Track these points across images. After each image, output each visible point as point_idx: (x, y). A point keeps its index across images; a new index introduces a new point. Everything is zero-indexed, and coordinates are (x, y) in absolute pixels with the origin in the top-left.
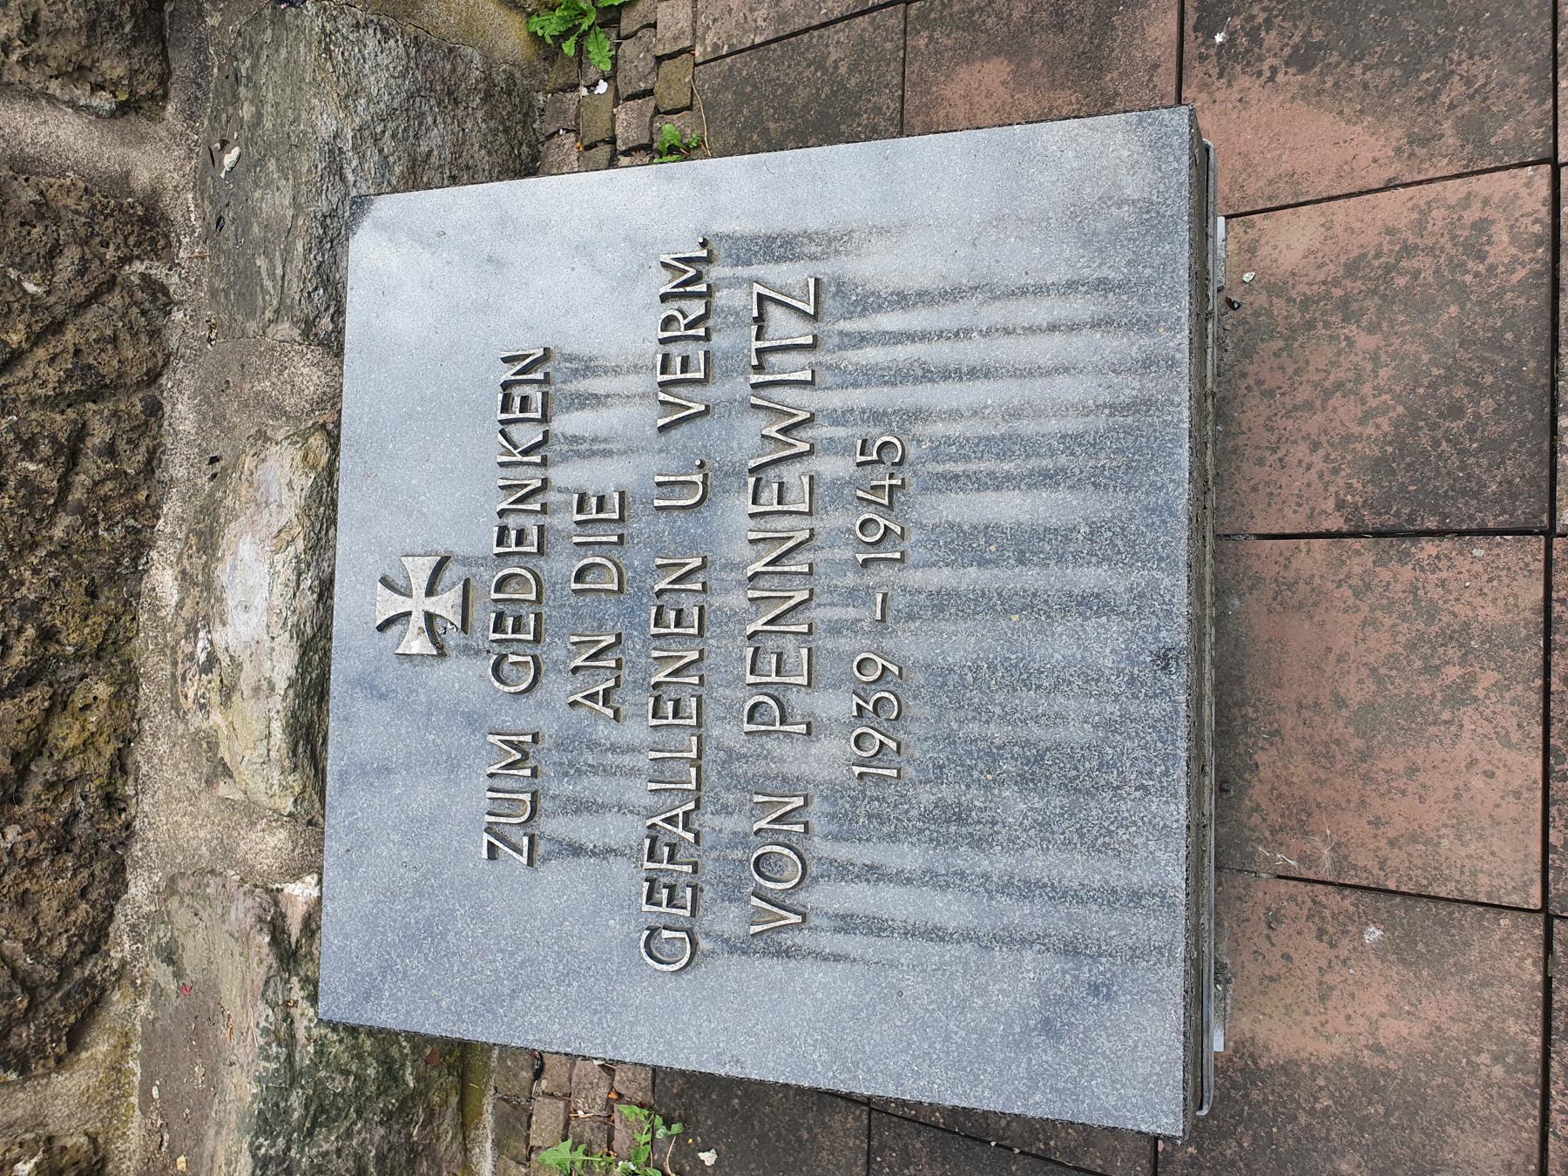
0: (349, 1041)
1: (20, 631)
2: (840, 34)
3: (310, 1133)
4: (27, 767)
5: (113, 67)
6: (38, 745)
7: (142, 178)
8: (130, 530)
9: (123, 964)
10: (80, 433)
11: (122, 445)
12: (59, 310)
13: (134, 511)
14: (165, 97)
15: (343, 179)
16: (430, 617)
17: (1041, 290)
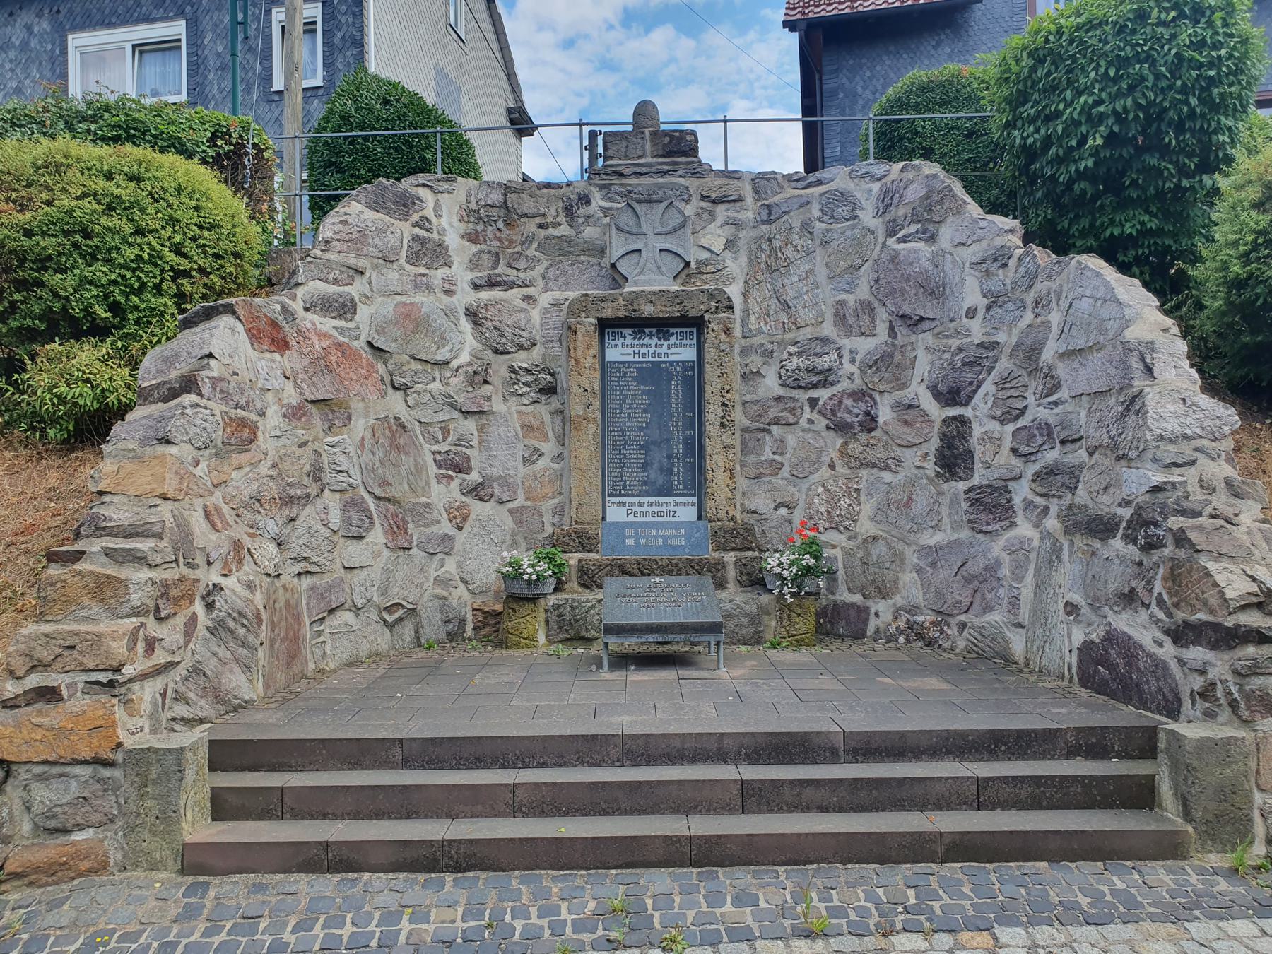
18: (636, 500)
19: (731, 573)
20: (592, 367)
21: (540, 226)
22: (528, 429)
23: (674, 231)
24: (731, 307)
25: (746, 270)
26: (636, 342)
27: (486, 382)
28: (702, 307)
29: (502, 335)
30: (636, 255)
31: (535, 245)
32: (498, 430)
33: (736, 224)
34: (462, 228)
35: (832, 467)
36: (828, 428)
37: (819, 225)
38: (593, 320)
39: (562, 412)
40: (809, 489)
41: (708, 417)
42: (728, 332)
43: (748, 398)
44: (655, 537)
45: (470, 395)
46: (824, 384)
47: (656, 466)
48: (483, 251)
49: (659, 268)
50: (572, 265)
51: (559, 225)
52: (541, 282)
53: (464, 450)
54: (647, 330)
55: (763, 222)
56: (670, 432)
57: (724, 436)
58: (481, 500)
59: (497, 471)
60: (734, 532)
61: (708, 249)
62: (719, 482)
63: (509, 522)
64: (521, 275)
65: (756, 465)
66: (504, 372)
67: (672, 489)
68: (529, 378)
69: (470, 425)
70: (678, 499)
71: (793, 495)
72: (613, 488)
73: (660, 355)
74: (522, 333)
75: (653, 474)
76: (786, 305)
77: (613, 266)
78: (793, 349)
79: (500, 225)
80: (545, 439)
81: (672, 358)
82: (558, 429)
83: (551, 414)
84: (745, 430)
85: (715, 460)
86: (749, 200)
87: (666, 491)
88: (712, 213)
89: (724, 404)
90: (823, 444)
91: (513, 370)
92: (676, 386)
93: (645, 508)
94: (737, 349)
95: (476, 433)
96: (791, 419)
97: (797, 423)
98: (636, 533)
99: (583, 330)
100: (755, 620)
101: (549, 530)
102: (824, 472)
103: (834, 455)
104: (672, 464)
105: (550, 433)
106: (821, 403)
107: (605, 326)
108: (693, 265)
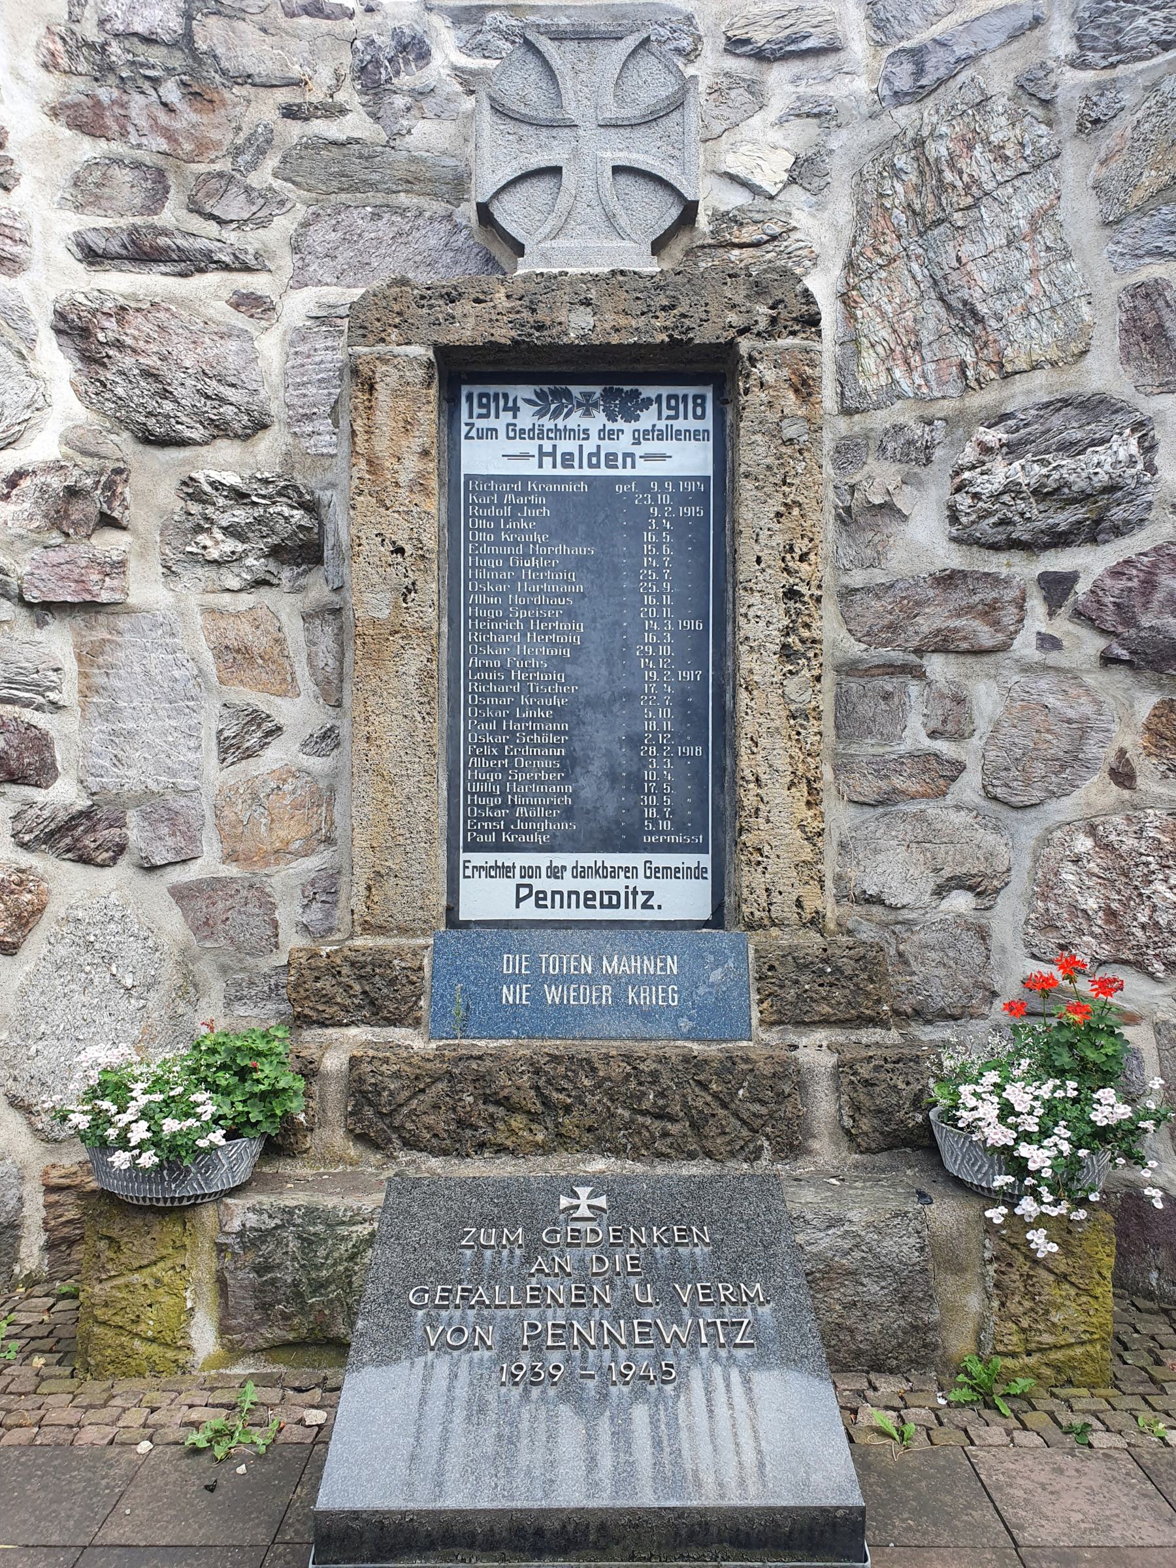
0: (346, 1255)
1: (569, 1096)
2: (990, 1515)
3: (300, 1237)
4: (501, 1105)
5: (865, 1124)
6: (512, 1108)
7: (815, 1145)
8: (625, 1146)
9: (395, 1158)
10: (673, 1119)
11: (669, 1140)
12: (733, 1106)
13: (635, 1148)
14: (861, 1152)
15: (829, 1227)
16: (577, 1207)
17: (756, 1438)
18: (541, 860)
19: (824, 1106)
20: (419, 485)
21: (290, 112)
22: (236, 657)
23: (651, 119)
24: (812, 321)
25: (848, 233)
26: (547, 423)
27: (108, 521)
28: (732, 317)
29: (165, 394)
30: (544, 185)
31: (272, 162)
32: (135, 656)
33: (821, 115)
34: (52, 86)
35: (1123, 775)
36: (1108, 660)
37: (1073, 77)
38: (421, 351)
39: (337, 612)
40: (1046, 841)
41: (747, 628)
42: (804, 388)
43: (857, 578)
44: (590, 980)
45: (54, 557)
46: (1093, 532)
48: (118, 161)
49: (610, 218)
50: (375, 216)
51: (343, 111)
52: (286, 262)
53: (28, 715)
54: (576, 390)
55: (899, 97)
57: (792, 685)
58: (85, 860)
59: (136, 775)
60: (825, 969)
61: (744, 184)
62: (776, 814)
63: (173, 924)
64: (231, 236)
65: (881, 767)
66: (168, 496)
68: (241, 515)
69: (57, 643)
70: (661, 860)
71: (990, 856)
72: (481, 825)
73: (611, 459)
74: (228, 393)
75: (589, 786)
76: (968, 317)
77: (484, 211)
78: (993, 436)
79: (171, 92)
80: (287, 688)
81: (644, 469)
82: (326, 660)
83: (306, 617)
84: (849, 668)
85: (766, 751)
86: (858, 47)
87: (625, 837)
88: (753, 88)
89: (791, 594)
90: (1088, 709)
91: (192, 491)
92: (657, 549)
93: (567, 883)
94: (828, 440)
95: (71, 666)
96: (986, 636)
97: (1004, 648)
98: (534, 964)
99: (393, 380)
100: (912, 1287)
101: (292, 941)
102: (1096, 791)
103: (1131, 740)
104: (644, 763)
105: (302, 672)
106: (1082, 587)
108: (703, 221)
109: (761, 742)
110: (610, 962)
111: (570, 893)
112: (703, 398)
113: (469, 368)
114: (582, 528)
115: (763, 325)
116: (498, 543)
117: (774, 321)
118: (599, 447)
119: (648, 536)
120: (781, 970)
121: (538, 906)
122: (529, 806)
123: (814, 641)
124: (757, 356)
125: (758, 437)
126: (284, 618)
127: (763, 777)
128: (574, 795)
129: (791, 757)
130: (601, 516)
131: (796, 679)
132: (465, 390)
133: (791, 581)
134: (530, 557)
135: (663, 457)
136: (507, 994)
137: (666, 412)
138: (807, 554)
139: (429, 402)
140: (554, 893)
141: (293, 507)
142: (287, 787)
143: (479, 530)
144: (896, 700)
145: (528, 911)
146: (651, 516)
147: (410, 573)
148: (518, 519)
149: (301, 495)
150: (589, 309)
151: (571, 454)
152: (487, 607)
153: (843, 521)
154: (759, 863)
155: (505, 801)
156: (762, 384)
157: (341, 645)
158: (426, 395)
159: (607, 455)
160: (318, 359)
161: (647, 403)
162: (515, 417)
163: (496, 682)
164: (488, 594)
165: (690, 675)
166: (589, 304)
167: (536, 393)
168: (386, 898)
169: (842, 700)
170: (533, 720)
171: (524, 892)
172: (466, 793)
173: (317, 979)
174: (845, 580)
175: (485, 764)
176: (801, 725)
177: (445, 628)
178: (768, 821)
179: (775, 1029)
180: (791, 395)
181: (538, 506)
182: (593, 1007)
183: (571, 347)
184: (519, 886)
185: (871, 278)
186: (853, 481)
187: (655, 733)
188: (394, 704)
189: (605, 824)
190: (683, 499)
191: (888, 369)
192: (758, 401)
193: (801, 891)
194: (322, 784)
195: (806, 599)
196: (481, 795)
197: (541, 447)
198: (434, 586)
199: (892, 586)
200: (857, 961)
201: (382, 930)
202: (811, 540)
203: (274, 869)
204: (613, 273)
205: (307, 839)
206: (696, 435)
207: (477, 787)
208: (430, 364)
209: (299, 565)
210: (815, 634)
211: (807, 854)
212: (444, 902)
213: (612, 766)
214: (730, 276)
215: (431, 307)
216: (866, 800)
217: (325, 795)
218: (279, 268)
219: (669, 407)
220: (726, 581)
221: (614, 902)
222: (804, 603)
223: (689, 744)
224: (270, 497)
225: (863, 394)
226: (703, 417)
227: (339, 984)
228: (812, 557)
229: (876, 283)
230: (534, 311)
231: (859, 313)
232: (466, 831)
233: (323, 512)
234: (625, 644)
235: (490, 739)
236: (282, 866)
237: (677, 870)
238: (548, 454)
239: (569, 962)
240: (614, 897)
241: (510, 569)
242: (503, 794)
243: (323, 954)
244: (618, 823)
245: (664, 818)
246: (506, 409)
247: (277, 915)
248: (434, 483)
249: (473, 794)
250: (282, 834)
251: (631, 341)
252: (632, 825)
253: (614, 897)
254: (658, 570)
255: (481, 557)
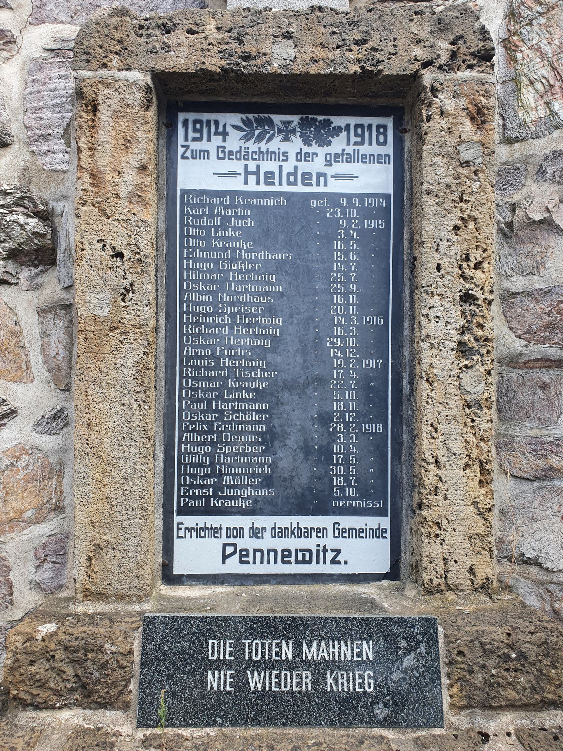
20: (136, 196)
26: (252, 146)
39: (68, 307)
41: (428, 328)
43: (518, 284)
47: (292, 441)
54: (277, 119)
56: (327, 361)
57: (467, 378)
67: (331, 497)
70: (347, 522)
72: (191, 492)
73: (307, 178)
75: (286, 459)
80: (23, 374)
81: (335, 187)
82: (57, 349)
83: (42, 312)
84: (512, 361)
92: (345, 257)
98: (239, 648)
99: (114, 102)
104: (333, 438)
105: (36, 360)
107: (181, 99)
109: (441, 428)
110: (309, 648)
111: (269, 551)
112: (385, 127)
113: (187, 98)
114: (281, 237)
115: (444, 58)
116: (208, 249)
117: (454, 55)
118: (296, 167)
119: (338, 245)
120: (469, 656)
121: (241, 562)
122: (234, 475)
123: (487, 340)
124: (439, 87)
125: (439, 159)
126: (21, 313)
127: (442, 459)
128: (273, 466)
129: (466, 442)
130: (297, 228)
131: (471, 373)
132: (182, 116)
133: (467, 286)
134: (236, 261)
135: (350, 177)
136: (213, 681)
137: (353, 139)
138: (481, 263)
139: (146, 123)
140: (255, 551)
141: (29, 216)
142: (21, 464)
143: (193, 237)
144: (553, 390)
145: (233, 566)
146: (339, 227)
147: (128, 276)
148: (226, 229)
149: (36, 205)
150: (290, 42)
151: (272, 173)
152: (199, 303)
153: (505, 235)
154: (437, 536)
155: (214, 470)
156: (442, 113)
157: (71, 336)
158: (144, 117)
159: (303, 174)
160: (52, 86)
161: (338, 130)
162: (224, 140)
163: (207, 368)
164: (201, 293)
165: (372, 363)
166: (290, 38)
167: (243, 120)
168: (105, 568)
169: (504, 388)
170: (239, 400)
171: (229, 550)
172: (180, 463)
173: (32, 663)
174: (507, 285)
175: (197, 438)
176: (475, 414)
177: (162, 321)
178: (446, 498)
179: (464, 712)
180: (468, 122)
181: (243, 218)
182: (293, 693)
183: (274, 75)
184: (225, 545)
185: (531, 24)
186: (513, 201)
187: (343, 413)
188: (112, 393)
189: (299, 490)
190: (366, 213)
191: (547, 103)
192: (438, 127)
193: (474, 560)
194: (53, 460)
195: (480, 302)
196: (192, 465)
197: (246, 166)
198: (151, 287)
199: (549, 291)
200: (539, 646)
201: (101, 596)
202: (485, 251)
203: (9, 536)
204: (312, 9)
205: (39, 508)
206: (379, 159)
207: (190, 459)
208: (148, 90)
209: (36, 266)
210: (488, 333)
211: (479, 528)
212: (160, 560)
213: (306, 440)
214: (416, 13)
215: (149, 36)
216: (526, 476)
217: (54, 470)
218: (19, 6)
219: (356, 135)
220: (403, 283)
221: (307, 558)
222: (478, 306)
223: (371, 422)
224: (8, 207)
225: (523, 126)
226: (385, 143)
227: (53, 668)
228: (485, 265)
229: (536, 28)
230: (241, 42)
231: (519, 55)
232: (179, 497)
233: (56, 220)
234: (317, 336)
235: (201, 416)
236: (16, 533)
237: (361, 530)
238: (252, 173)
239: (270, 649)
240: (307, 554)
241: (220, 271)
242: (212, 464)
243: (39, 637)
244: (310, 489)
245: (350, 486)
246: (217, 133)
247: (11, 577)
248: (151, 195)
249: (186, 465)
250: (16, 505)
251: (328, 71)
252: (323, 491)
253: (307, 554)
254: (346, 274)
255: (195, 260)
